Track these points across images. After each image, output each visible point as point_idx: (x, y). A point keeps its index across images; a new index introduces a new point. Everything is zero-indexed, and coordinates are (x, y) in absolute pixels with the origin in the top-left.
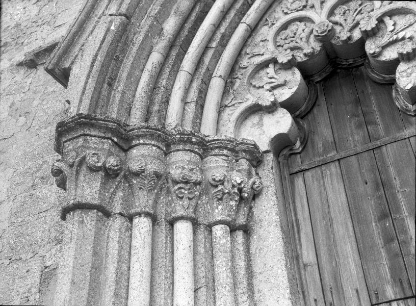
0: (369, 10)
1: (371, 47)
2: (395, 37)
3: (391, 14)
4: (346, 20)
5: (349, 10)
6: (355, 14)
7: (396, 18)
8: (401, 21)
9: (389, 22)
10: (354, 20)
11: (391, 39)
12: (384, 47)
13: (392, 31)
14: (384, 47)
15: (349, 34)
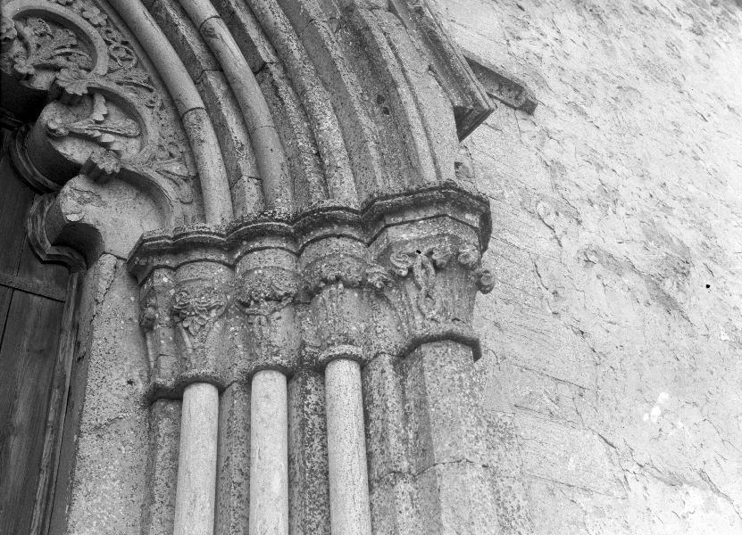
0: (83, 65)
1: (52, 117)
2: (97, 134)
3: (112, 98)
4: (39, 46)
5: (52, 37)
6: (58, 52)
7: (113, 110)
8: (118, 121)
9: (101, 109)
10: (52, 58)
11: (90, 133)
12: (73, 135)
13: (97, 122)
14: (73, 135)
15: (32, 71)
